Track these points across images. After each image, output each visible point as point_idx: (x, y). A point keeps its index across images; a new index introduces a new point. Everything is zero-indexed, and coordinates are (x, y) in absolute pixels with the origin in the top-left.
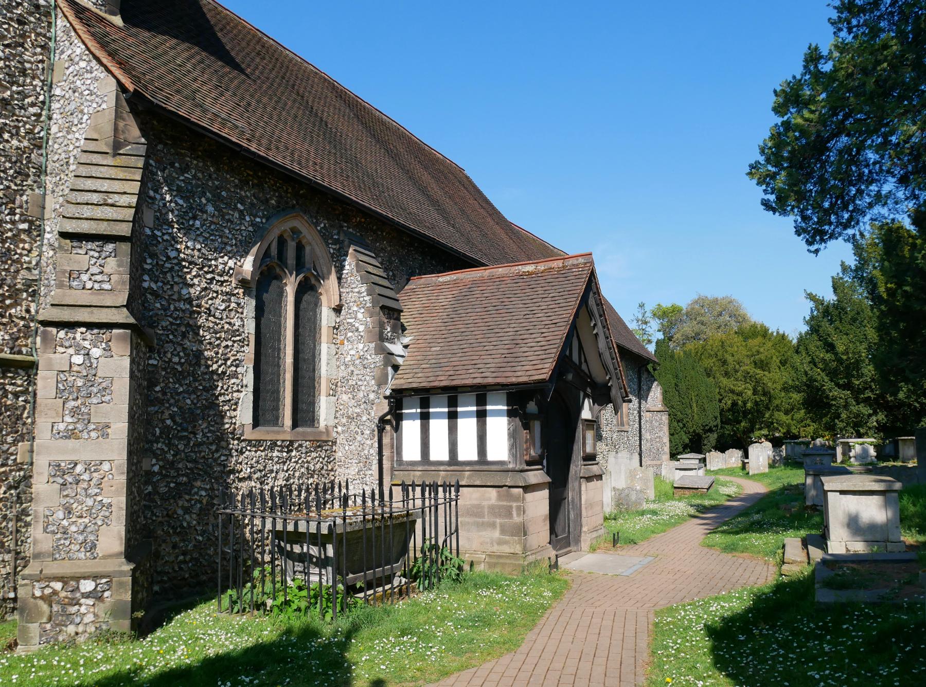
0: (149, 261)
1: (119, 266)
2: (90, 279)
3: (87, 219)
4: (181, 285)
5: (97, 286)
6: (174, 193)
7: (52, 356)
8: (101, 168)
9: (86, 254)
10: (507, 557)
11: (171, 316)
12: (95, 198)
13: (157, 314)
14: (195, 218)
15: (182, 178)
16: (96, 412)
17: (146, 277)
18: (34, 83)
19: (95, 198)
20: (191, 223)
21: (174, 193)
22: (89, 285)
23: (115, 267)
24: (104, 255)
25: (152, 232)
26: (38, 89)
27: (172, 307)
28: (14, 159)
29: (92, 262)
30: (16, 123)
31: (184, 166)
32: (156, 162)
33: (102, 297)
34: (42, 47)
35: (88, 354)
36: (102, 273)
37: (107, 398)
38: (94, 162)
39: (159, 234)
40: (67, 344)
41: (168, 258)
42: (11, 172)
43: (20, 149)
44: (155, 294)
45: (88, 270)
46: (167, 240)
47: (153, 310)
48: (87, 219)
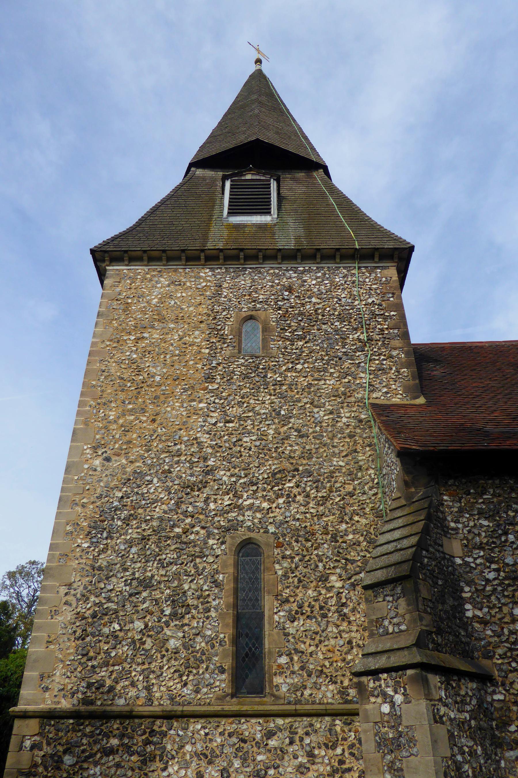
0: (467, 589)
4: (511, 605)
11: (507, 641)
13: (490, 643)
14: (506, 533)
16: (407, 767)
17: (468, 606)
18: (369, 473)
19: (390, 547)
20: (503, 539)
22: (391, 630)
23: (406, 607)
25: (463, 560)
27: (506, 631)
31: (480, 490)
34: (369, 446)
35: (392, 701)
39: (470, 560)
41: (488, 581)
44: (484, 622)
46: (481, 564)
47: (484, 639)
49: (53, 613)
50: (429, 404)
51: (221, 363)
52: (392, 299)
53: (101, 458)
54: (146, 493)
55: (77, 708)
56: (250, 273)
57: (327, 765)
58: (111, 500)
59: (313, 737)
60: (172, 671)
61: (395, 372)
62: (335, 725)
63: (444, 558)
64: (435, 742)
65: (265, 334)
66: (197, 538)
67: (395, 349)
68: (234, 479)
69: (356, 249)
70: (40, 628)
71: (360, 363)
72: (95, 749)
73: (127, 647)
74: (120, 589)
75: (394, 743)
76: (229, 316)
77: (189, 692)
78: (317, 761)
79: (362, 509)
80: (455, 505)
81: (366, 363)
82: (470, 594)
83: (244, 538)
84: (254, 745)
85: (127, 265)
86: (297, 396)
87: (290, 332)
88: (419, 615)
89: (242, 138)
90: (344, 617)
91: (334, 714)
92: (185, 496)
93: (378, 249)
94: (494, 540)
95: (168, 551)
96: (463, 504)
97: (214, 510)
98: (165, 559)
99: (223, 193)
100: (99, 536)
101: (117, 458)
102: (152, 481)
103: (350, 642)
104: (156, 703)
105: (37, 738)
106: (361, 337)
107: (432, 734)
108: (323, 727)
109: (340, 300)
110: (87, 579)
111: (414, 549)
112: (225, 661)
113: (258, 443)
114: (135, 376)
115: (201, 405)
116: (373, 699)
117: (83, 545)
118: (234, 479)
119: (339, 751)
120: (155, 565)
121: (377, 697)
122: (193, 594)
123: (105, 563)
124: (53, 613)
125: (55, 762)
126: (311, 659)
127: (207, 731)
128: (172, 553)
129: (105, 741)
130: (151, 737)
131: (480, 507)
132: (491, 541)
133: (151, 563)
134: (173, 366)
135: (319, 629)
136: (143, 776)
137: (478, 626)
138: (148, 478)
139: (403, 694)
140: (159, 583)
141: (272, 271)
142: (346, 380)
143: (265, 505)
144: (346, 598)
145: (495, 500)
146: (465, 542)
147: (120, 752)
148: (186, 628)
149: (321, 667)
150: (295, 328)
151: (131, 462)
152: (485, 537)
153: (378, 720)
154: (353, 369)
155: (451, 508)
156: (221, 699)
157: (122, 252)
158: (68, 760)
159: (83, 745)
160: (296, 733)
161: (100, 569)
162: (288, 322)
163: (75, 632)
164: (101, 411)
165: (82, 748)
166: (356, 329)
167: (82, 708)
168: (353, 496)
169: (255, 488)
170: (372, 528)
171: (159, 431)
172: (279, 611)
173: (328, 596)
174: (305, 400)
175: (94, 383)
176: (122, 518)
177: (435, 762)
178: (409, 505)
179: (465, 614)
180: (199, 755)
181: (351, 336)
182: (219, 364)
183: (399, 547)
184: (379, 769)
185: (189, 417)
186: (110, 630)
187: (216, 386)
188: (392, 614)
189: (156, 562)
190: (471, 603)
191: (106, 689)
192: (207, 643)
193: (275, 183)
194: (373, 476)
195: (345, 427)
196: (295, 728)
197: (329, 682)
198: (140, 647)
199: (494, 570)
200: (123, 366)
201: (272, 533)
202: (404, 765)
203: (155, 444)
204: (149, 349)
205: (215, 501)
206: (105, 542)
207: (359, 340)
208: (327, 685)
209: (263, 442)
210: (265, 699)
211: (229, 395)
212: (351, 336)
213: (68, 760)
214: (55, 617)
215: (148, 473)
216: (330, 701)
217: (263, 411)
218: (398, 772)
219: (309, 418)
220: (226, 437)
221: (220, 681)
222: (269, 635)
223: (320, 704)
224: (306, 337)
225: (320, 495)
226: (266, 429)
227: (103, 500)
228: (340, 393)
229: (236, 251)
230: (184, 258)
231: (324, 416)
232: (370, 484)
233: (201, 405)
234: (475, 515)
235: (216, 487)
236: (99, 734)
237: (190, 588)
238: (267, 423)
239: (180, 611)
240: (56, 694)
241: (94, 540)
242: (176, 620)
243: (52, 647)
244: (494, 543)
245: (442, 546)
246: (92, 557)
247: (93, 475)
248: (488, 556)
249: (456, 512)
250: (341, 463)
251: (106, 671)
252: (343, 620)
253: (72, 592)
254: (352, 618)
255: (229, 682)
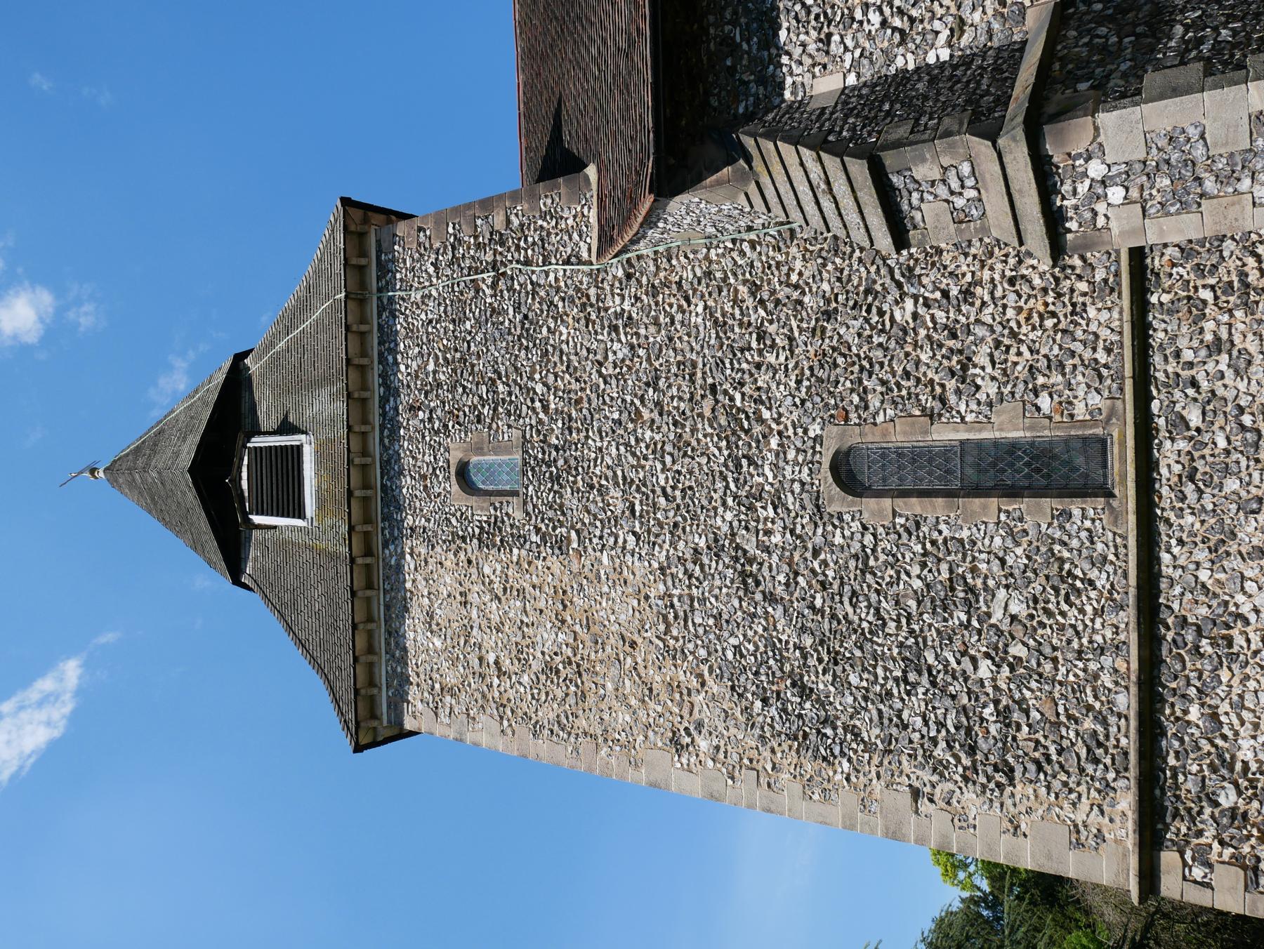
0: (900, 62)
1: (924, 160)
2: (961, 194)
3: (863, 219)
5: (970, 182)
6: (774, 51)
7: (1115, 231)
8: (782, 191)
9: (919, 209)
10: (384, 376)
12: (827, 204)
15: (745, 46)
18: (715, 258)
19: (827, 204)
21: (774, 51)
22: (972, 194)
23: (927, 165)
24: (912, 186)
25: (849, 71)
26: (720, 251)
28: (820, 261)
29: (931, 198)
30: (774, 268)
32: (739, 102)
33: (987, 176)
35: (1103, 182)
36: (944, 181)
37: (1193, 132)
38: (776, 200)
39: (848, 57)
40: (1088, 215)
42: (838, 261)
43: (804, 256)
45: (947, 201)
48: (863, 219)
49: (965, 825)
50: (597, 158)
51: (535, 527)
52: (428, 233)
53: (696, 737)
54: (756, 658)
55: (1132, 781)
56: (390, 479)
57: (1232, 316)
58: (769, 720)
59: (1182, 343)
60: (1065, 607)
61: (545, 219)
62: (1161, 304)
63: (846, 103)
64: (1176, 92)
65: (486, 450)
66: (832, 565)
67: (508, 221)
68: (730, 501)
69: (346, 297)
70: (990, 848)
71: (532, 283)
72: (1206, 747)
73: (1025, 691)
74: (923, 704)
75: (1179, 175)
76: (458, 514)
77: (1104, 575)
78: (1225, 336)
79: (778, 268)
80: (753, 90)
81: (533, 272)
82: (909, 56)
83: (830, 479)
84: (1200, 453)
85: (380, 689)
86: (588, 392)
87: (483, 406)
88: (940, 138)
89: (191, 497)
90: (967, 293)
91: (1140, 307)
92: (761, 588)
93: (345, 259)
94: (812, 17)
95: (856, 618)
96: (752, 77)
97: (783, 536)
98: (870, 623)
99: (275, 527)
100: (829, 741)
101: (696, 710)
102: (735, 647)
103: (1012, 281)
104: (1122, 637)
105: (1188, 855)
106: (489, 281)
107: (1162, 97)
108: (1163, 325)
109: (431, 321)
110: (905, 763)
111: (822, 154)
112: (1049, 510)
113: (668, 459)
114: (558, 678)
115: (605, 560)
116: (1101, 221)
117: (846, 770)
118: (730, 501)
119: (1206, 295)
120: (880, 641)
121: (1095, 214)
122: (930, 571)
123: (877, 731)
124: (965, 825)
125: (1232, 823)
126: (1043, 352)
127: (1174, 542)
128: (858, 611)
129: (1193, 730)
130: (1186, 644)
131: (755, 47)
132: (813, 23)
133: (876, 647)
134: (541, 611)
135: (989, 340)
136: (1257, 660)
137: (966, 35)
138: (730, 655)
139: (1086, 161)
140: (912, 632)
141: (386, 441)
142: (560, 304)
143: (774, 442)
144: (933, 292)
145: (743, 20)
146: (817, 69)
147: (1212, 702)
148: (991, 583)
149: (1056, 332)
150: (476, 400)
151: (703, 684)
152: (807, 33)
153: (1138, 207)
154: (542, 293)
155: (758, 98)
156: (1116, 517)
157: (359, 698)
158: (1228, 798)
159: (1202, 770)
160: (1178, 375)
161: (889, 739)
162: (467, 410)
163: (999, 785)
164: (617, 737)
165: (1206, 773)
166: (477, 291)
167: (1133, 772)
168: (756, 285)
169: (744, 462)
170: (811, 248)
171: (649, 634)
172: (958, 412)
173: (931, 325)
174: (595, 376)
175: (570, 749)
176: (799, 700)
177: (1215, 87)
178: (756, 174)
179: (945, 62)
180: (1217, 552)
181: (489, 300)
182: (538, 530)
183: (823, 186)
184: (1233, 204)
185: (625, 582)
186: (996, 722)
187: (573, 534)
188: (942, 191)
189: (875, 639)
190: (926, 53)
191: (1100, 728)
192: (1018, 544)
193: (253, 440)
194: (720, 251)
195: (639, 304)
196: (1168, 377)
197: (1082, 318)
198: (1025, 668)
199: (865, 13)
200: (543, 698)
201: (822, 429)
202: (1222, 151)
203: (672, 642)
204: (514, 653)
205: (768, 533)
206: (840, 731)
207: (494, 286)
208: (1089, 320)
209: (668, 448)
210: (1115, 434)
211: (589, 512)
212: (489, 300)
213: (1228, 798)
214: (971, 821)
215: (720, 653)
216: (1116, 315)
217: (614, 452)
218: (1236, 164)
219: (625, 369)
220: (659, 516)
221: (1084, 517)
222: (1001, 430)
223: (1121, 333)
224: (490, 379)
225: (754, 345)
226: (643, 445)
227: (768, 735)
228: (582, 315)
229: (353, 502)
230: (369, 593)
231: (620, 341)
232: (735, 254)
233: (605, 560)
234: (770, 54)
235: (744, 532)
236: (1182, 741)
237: (919, 577)
238: (633, 443)
239: (962, 595)
240: (1107, 819)
241: (837, 750)
242: (977, 601)
243: (1023, 826)
244: (817, 17)
245: (824, 109)
246: (867, 755)
247: (726, 752)
248: (841, 26)
249: (765, 89)
250: (700, 309)
251: (1068, 728)
252: (973, 295)
253: (927, 789)
254: (969, 278)
255: (1085, 502)
